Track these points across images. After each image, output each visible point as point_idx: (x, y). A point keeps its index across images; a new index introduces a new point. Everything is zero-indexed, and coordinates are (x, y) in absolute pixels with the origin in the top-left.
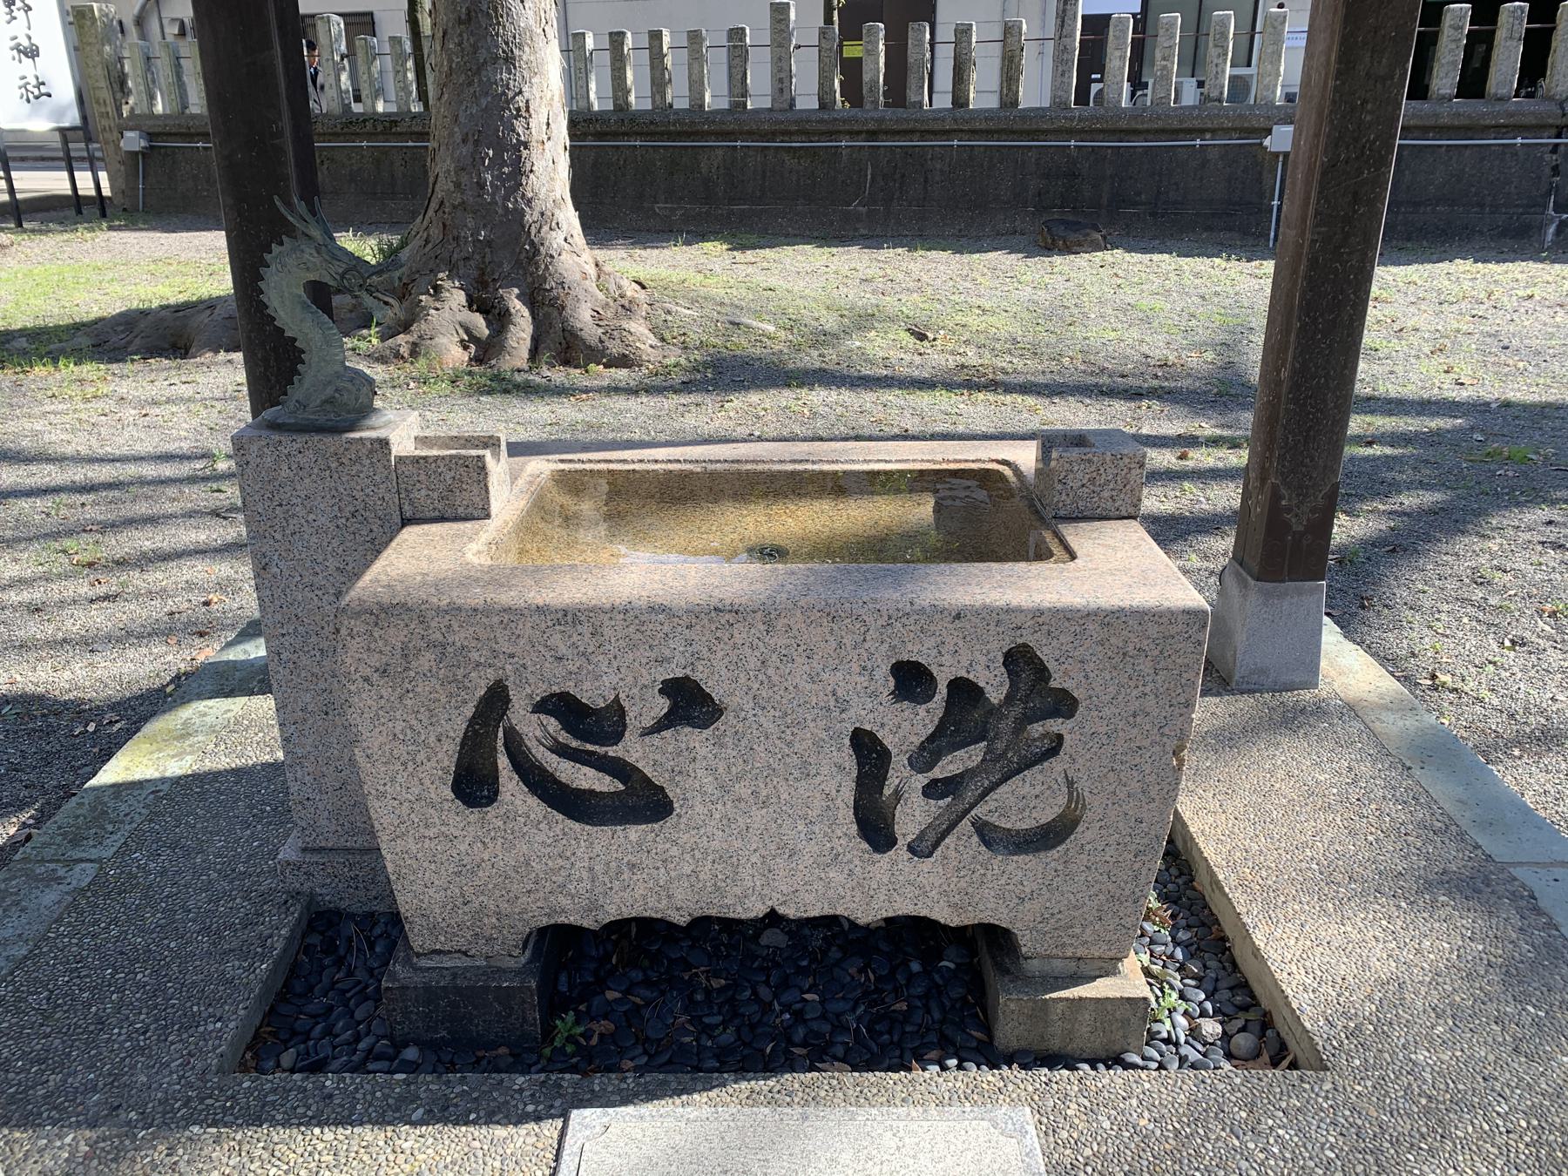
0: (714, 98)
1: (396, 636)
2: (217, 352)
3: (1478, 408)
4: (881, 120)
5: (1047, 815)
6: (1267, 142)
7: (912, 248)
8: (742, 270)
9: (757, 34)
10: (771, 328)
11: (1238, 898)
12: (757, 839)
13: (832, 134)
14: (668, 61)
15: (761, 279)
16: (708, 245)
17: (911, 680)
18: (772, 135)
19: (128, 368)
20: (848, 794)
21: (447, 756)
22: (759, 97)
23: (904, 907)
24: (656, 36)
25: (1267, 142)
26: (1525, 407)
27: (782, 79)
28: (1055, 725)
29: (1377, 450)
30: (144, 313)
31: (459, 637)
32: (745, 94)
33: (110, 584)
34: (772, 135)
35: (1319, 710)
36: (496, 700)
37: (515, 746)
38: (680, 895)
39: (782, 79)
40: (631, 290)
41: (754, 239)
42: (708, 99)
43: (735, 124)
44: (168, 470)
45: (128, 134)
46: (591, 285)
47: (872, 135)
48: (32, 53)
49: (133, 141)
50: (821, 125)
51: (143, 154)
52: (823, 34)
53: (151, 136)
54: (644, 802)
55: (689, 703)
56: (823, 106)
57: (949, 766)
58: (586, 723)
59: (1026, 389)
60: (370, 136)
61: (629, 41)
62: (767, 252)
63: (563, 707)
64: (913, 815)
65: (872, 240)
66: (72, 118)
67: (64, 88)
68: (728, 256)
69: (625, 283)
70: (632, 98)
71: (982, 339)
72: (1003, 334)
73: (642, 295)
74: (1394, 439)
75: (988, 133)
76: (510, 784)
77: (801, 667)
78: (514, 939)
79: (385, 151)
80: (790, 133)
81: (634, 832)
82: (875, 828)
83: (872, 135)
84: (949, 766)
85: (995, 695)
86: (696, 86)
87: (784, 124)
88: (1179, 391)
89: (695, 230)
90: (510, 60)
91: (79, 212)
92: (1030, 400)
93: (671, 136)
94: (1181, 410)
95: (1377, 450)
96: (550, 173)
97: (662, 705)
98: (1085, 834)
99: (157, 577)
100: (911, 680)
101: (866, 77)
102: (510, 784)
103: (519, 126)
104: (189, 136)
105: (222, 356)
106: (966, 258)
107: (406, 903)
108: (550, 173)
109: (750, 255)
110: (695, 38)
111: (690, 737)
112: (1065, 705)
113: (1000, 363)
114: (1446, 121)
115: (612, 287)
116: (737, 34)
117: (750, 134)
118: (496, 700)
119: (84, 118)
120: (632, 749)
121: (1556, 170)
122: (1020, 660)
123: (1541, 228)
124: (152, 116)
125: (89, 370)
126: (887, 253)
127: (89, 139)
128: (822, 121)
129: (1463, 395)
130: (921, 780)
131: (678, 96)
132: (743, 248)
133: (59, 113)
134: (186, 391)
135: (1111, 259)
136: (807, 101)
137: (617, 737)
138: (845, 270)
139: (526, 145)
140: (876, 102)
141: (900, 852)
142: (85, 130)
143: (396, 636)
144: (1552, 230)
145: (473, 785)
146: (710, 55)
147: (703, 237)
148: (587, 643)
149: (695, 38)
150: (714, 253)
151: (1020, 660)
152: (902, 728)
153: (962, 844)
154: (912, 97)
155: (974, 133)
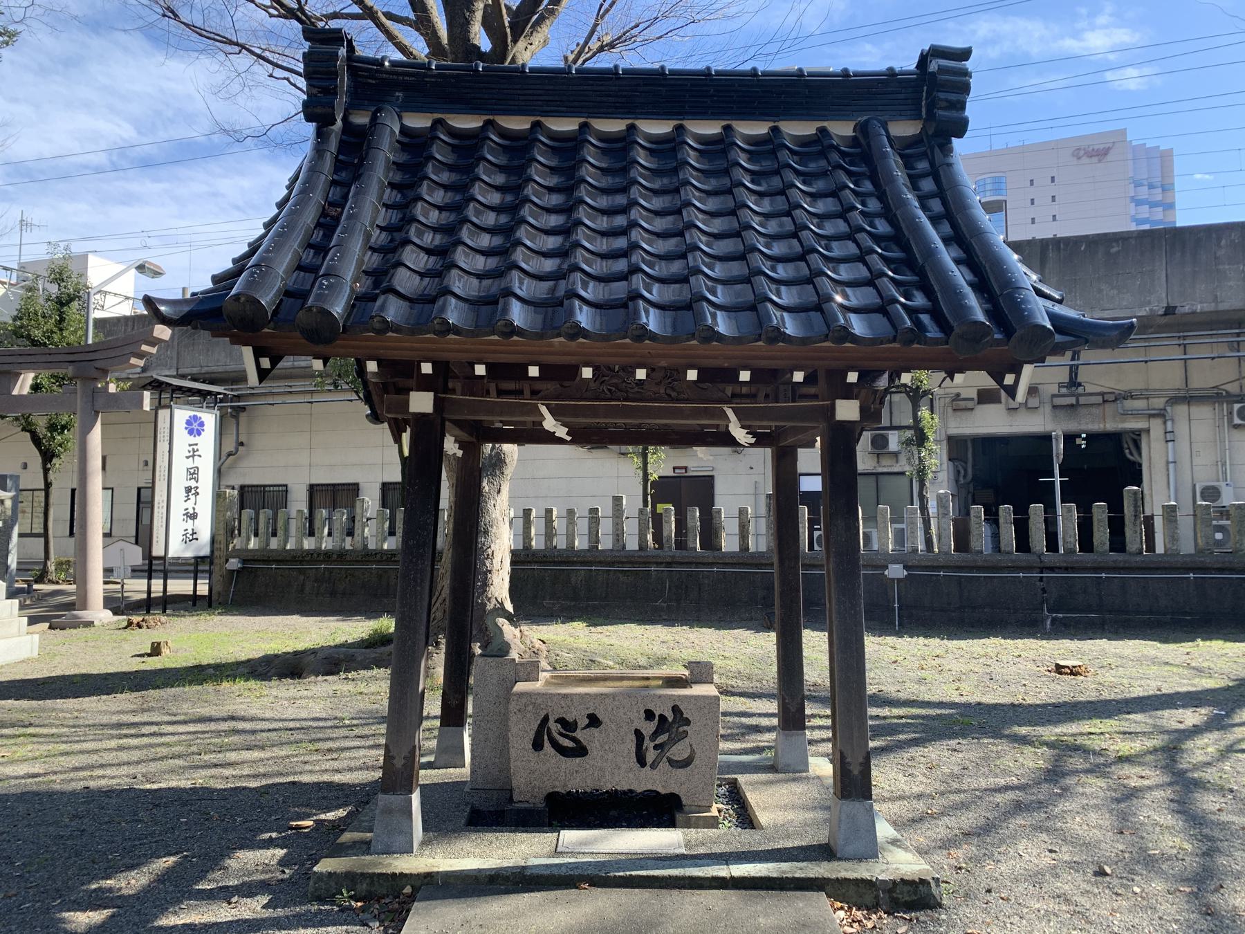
0: (580, 543)
1: (524, 700)
2: (317, 676)
3: (967, 705)
4: (673, 557)
5: (686, 756)
6: (886, 573)
7: (692, 627)
8: (595, 637)
9: (605, 509)
10: (611, 663)
11: (755, 808)
12: (610, 767)
13: (646, 564)
14: (555, 524)
15: (607, 641)
16: (575, 624)
17: (649, 715)
18: (612, 564)
19: (273, 683)
20: (634, 749)
21: (532, 735)
22: (606, 543)
23: (650, 787)
24: (549, 511)
25: (886, 573)
26: (988, 705)
27: (618, 534)
28: (685, 728)
29: (904, 721)
30: (276, 656)
31: (539, 701)
32: (598, 541)
33: (335, 755)
34: (612, 564)
35: (807, 778)
36: (546, 719)
37: (549, 729)
38: (589, 782)
39: (618, 534)
40: (538, 644)
41: (601, 620)
42: (577, 543)
43: (592, 557)
44: (314, 724)
45: (232, 560)
46: (518, 641)
47: (669, 564)
48: (193, 516)
49: (234, 564)
50: (642, 558)
51: (238, 571)
52: (641, 511)
53: (244, 561)
54: (580, 751)
55: (594, 721)
56: (641, 549)
57: (660, 740)
58: (568, 726)
59: (741, 695)
60: (378, 562)
61: (534, 514)
62: (609, 627)
63: (561, 721)
64: (651, 755)
65: (669, 621)
66: (206, 551)
67: (205, 535)
68: (587, 630)
69: (535, 640)
70: (533, 543)
71: (722, 671)
72: (734, 669)
73: (543, 647)
74: (913, 717)
75: (733, 565)
76: (547, 744)
77: (622, 711)
78: (542, 796)
79: (385, 571)
80: (623, 563)
81: (578, 760)
82: (641, 761)
83: (669, 564)
84: (660, 740)
85: (670, 719)
86: (570, 536)
87: (619, 557)
88: (820, 697)
89: (568, 615)
90: (486, 532)
91: (194, 605)
92: (742, 699)
93: (555, 563)
94: (816, 705)
95: (904, 721)
96: (500, 587)
97: (587, 721)
98: (696, 762)
99: (347, 754)
100: (649, 715)
101: (665, 534)
102: (547, 744)
103: (488, 563)
104: (267, 561)
105: (320, 678)
106: (722, 632)
107: (515, 783)
108: (500, 587)
109: (599, 629)
110: (571, 513)
111: (594, 730)
112: (688, 722)
113: (730, 682)
114: (980, 564)
115: (528, 642)
116: (594, 511)
117: (600, 563)
118: (546, 719)
119: (212, 552)
120: (579, 734)
121: (1044, 590)
122: (676, 709)
123: (1043, 621)
124: (248, 550)
125: (252, 684)
126: (677, 629)
127: (211, 563)
128: (640, 557)
129: (963, 700)
130: (652, 744)
131: (560, 542)
132: (595, 625)
133: (200, 548)
134: (308, 693)
135: (893, 655)
136: (632, 544)
137: (574, 731)
138: (653, 637)
139: (490, 572)
140: (670, 547)
141: (648, 768)
142: (208, 560)
143: (524, 700)
144: (1049, 623)
145: (537, 745)
146: (578, 521)
147: (571, 619)
148: (569, 703)
149: (571, 513)
150: (578, 627)
151: (676, 709)
152: (648, 728)
153: (664, 765)
154: (690, 545)
155: (726, 564)
